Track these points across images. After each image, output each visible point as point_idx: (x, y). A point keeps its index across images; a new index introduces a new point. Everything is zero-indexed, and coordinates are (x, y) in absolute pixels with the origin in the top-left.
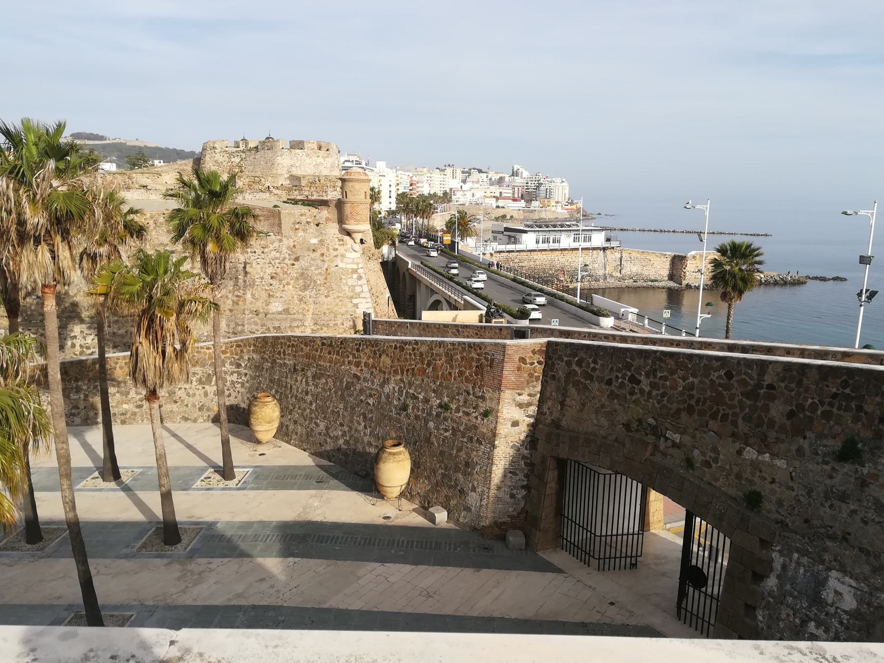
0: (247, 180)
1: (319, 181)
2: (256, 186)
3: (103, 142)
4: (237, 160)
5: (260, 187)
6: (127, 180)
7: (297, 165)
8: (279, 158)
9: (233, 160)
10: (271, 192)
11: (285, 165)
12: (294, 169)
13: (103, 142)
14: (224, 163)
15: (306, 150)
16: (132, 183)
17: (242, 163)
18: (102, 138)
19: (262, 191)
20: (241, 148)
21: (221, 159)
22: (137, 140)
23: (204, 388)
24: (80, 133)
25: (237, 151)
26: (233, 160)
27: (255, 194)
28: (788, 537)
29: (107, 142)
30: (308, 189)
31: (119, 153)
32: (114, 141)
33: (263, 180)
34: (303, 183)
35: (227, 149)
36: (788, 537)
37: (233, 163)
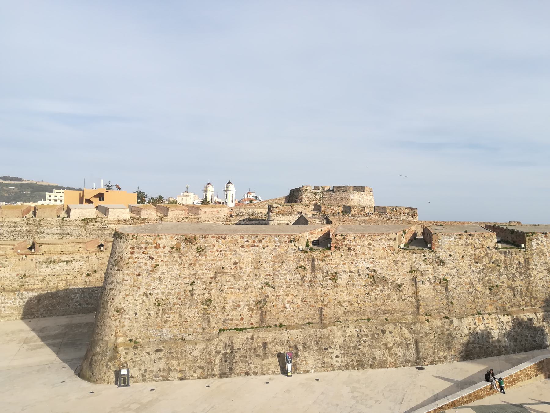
0: (357, 209)
1: (396, 210)
2: (362, 213)
3: (21, 182)
4: (318, 197)
5: (364, 213)
6: (291, 209)
7: (362, 200)
8: (352, 196)
9: (316, 197)
10: (370, 216)
11: (356, 200)
12: (361, 203)
13: (21, 182)
14: (312, 199)
15: (366, 191)
16: (294, 210)
17: (321, 199)
18: (20, 180)
19: (365, 216)
20: (320, 191)
21: (311, 197)
22: (42, 181)
23: (96, 254)
24: (6, 176)
25: (318, 192)
26: (316, 197)
27: (361, 217)
28: (394, 271)
29: (24, 182)
30: (390, 215)
31: (32, 189)
32: (28, 182)
33: (365, 209)
34: (388, 211)
35: (313, 191)
36: (394, 271)
37: (317, 199)
